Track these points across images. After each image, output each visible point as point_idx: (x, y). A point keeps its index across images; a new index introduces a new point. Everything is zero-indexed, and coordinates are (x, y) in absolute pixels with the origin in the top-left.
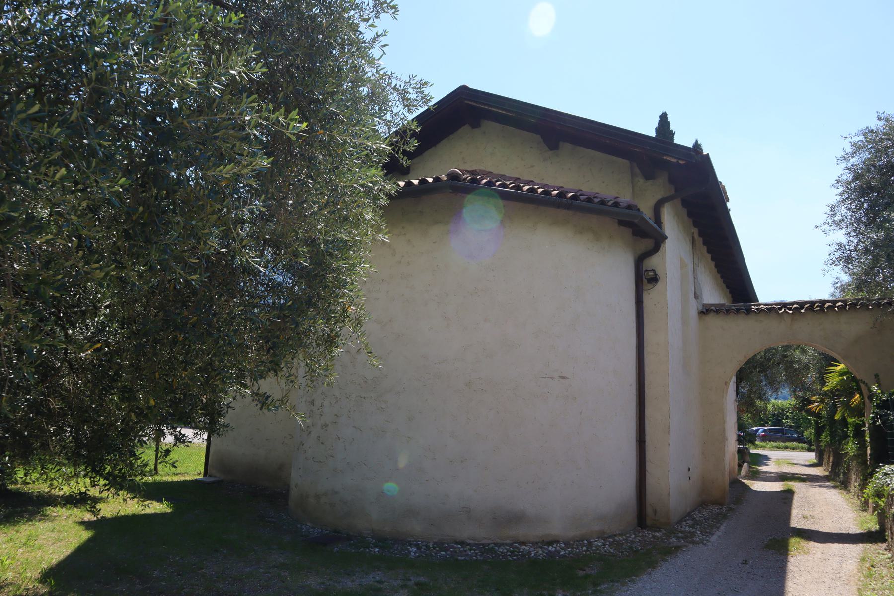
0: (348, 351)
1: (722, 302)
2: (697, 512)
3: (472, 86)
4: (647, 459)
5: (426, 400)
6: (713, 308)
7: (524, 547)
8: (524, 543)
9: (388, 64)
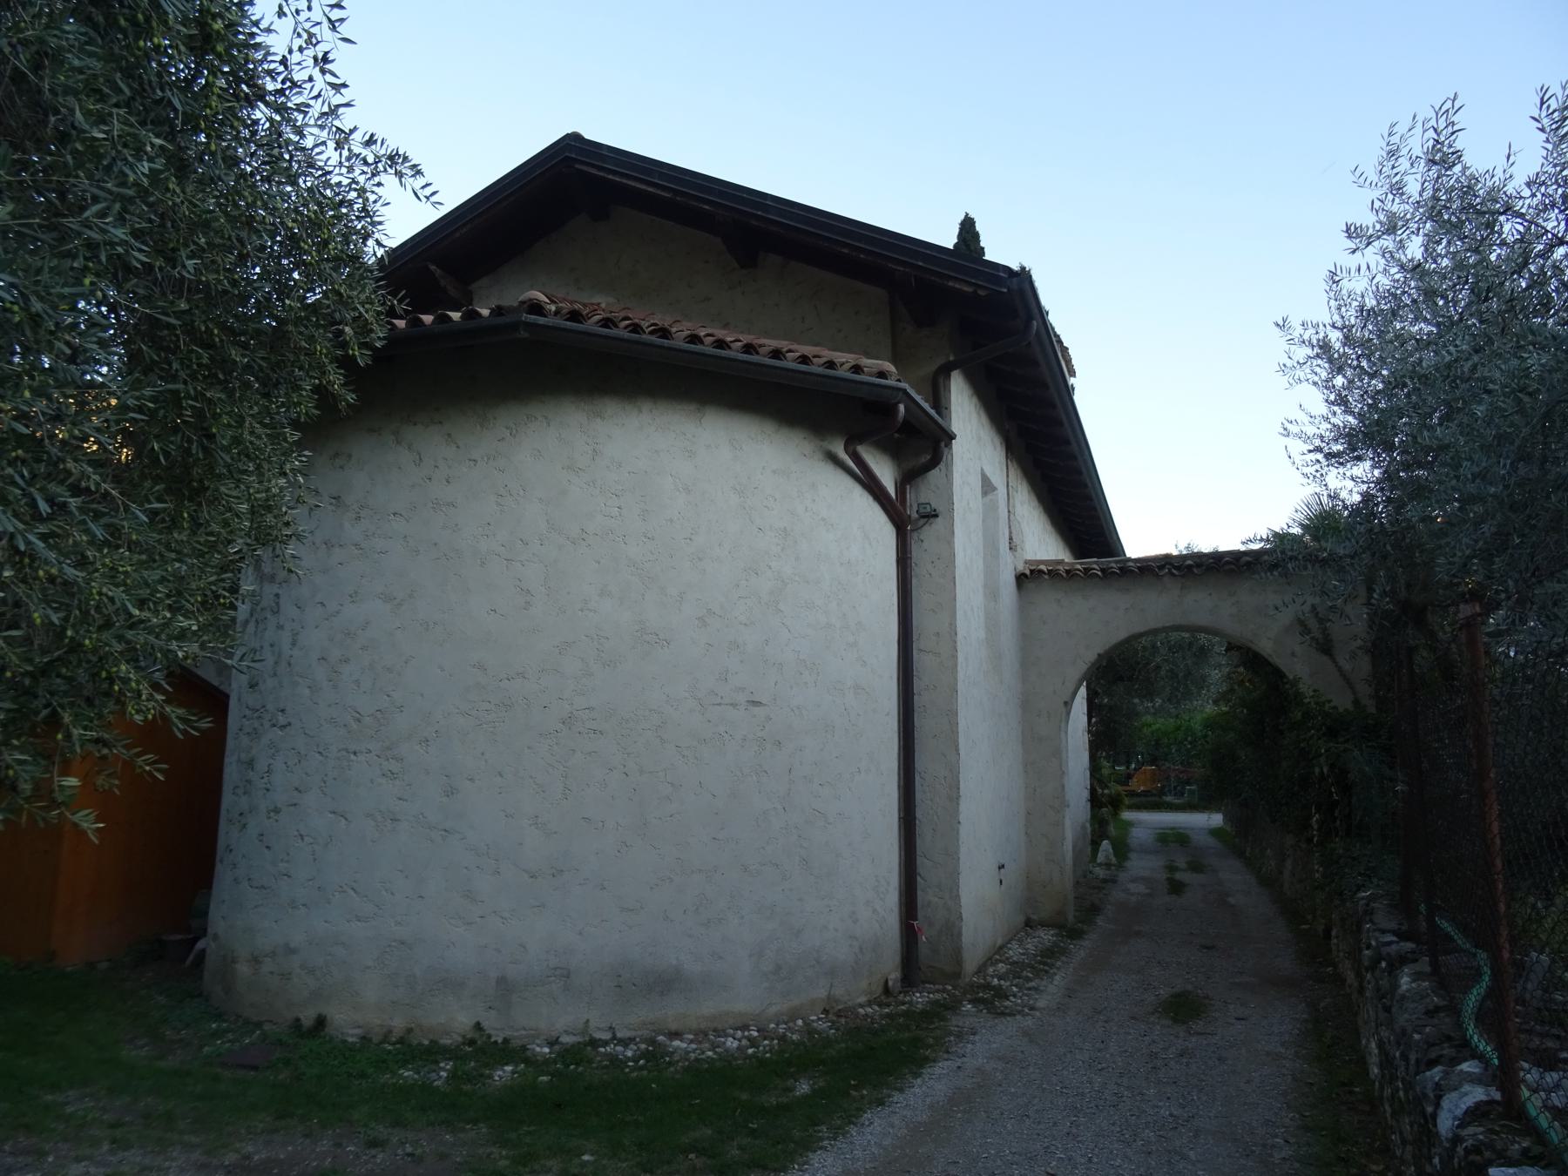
0: (323, 658)
1: (1060, 557)
2: (1015, 945)
3: (589, 135)
4: (919, 852)
5: (483, 754)
6: (1043, 567)
7: (677, 1043)
8: (676, 1035)
9: (1316, 402)
